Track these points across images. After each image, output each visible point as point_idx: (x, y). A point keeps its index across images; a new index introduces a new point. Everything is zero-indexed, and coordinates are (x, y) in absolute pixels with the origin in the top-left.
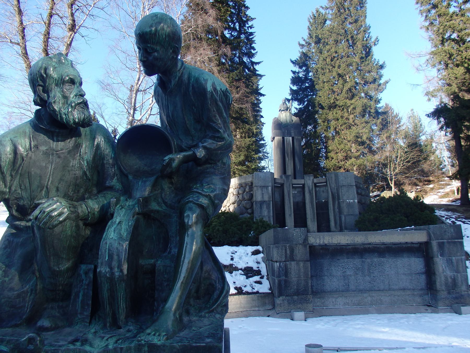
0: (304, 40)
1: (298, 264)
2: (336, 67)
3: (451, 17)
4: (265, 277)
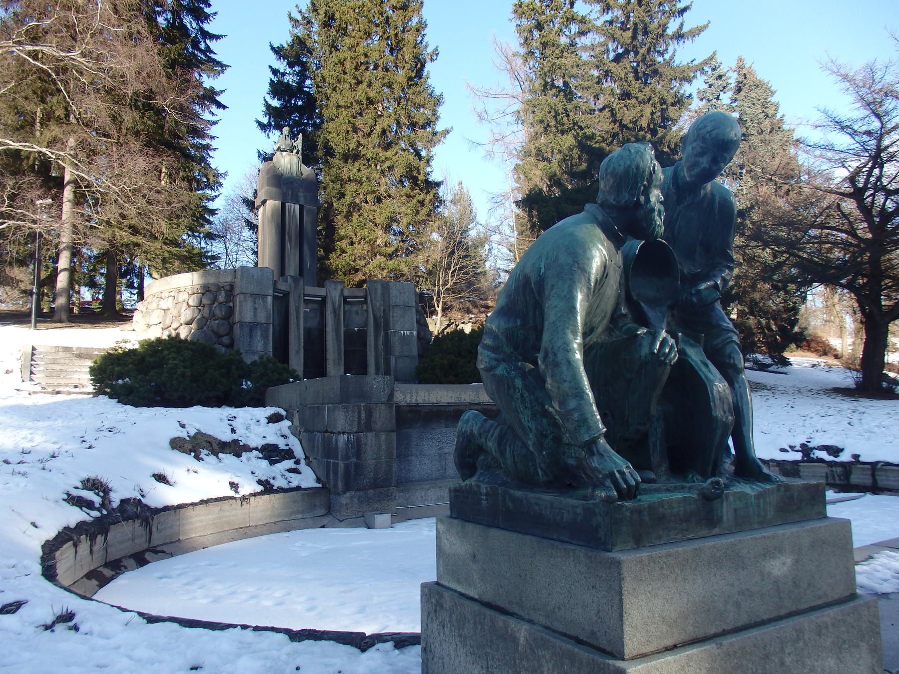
0: (300, 12)
1: (377, 437)
2: (365, 84)
3: (562, 52)
4: (303, 462)
